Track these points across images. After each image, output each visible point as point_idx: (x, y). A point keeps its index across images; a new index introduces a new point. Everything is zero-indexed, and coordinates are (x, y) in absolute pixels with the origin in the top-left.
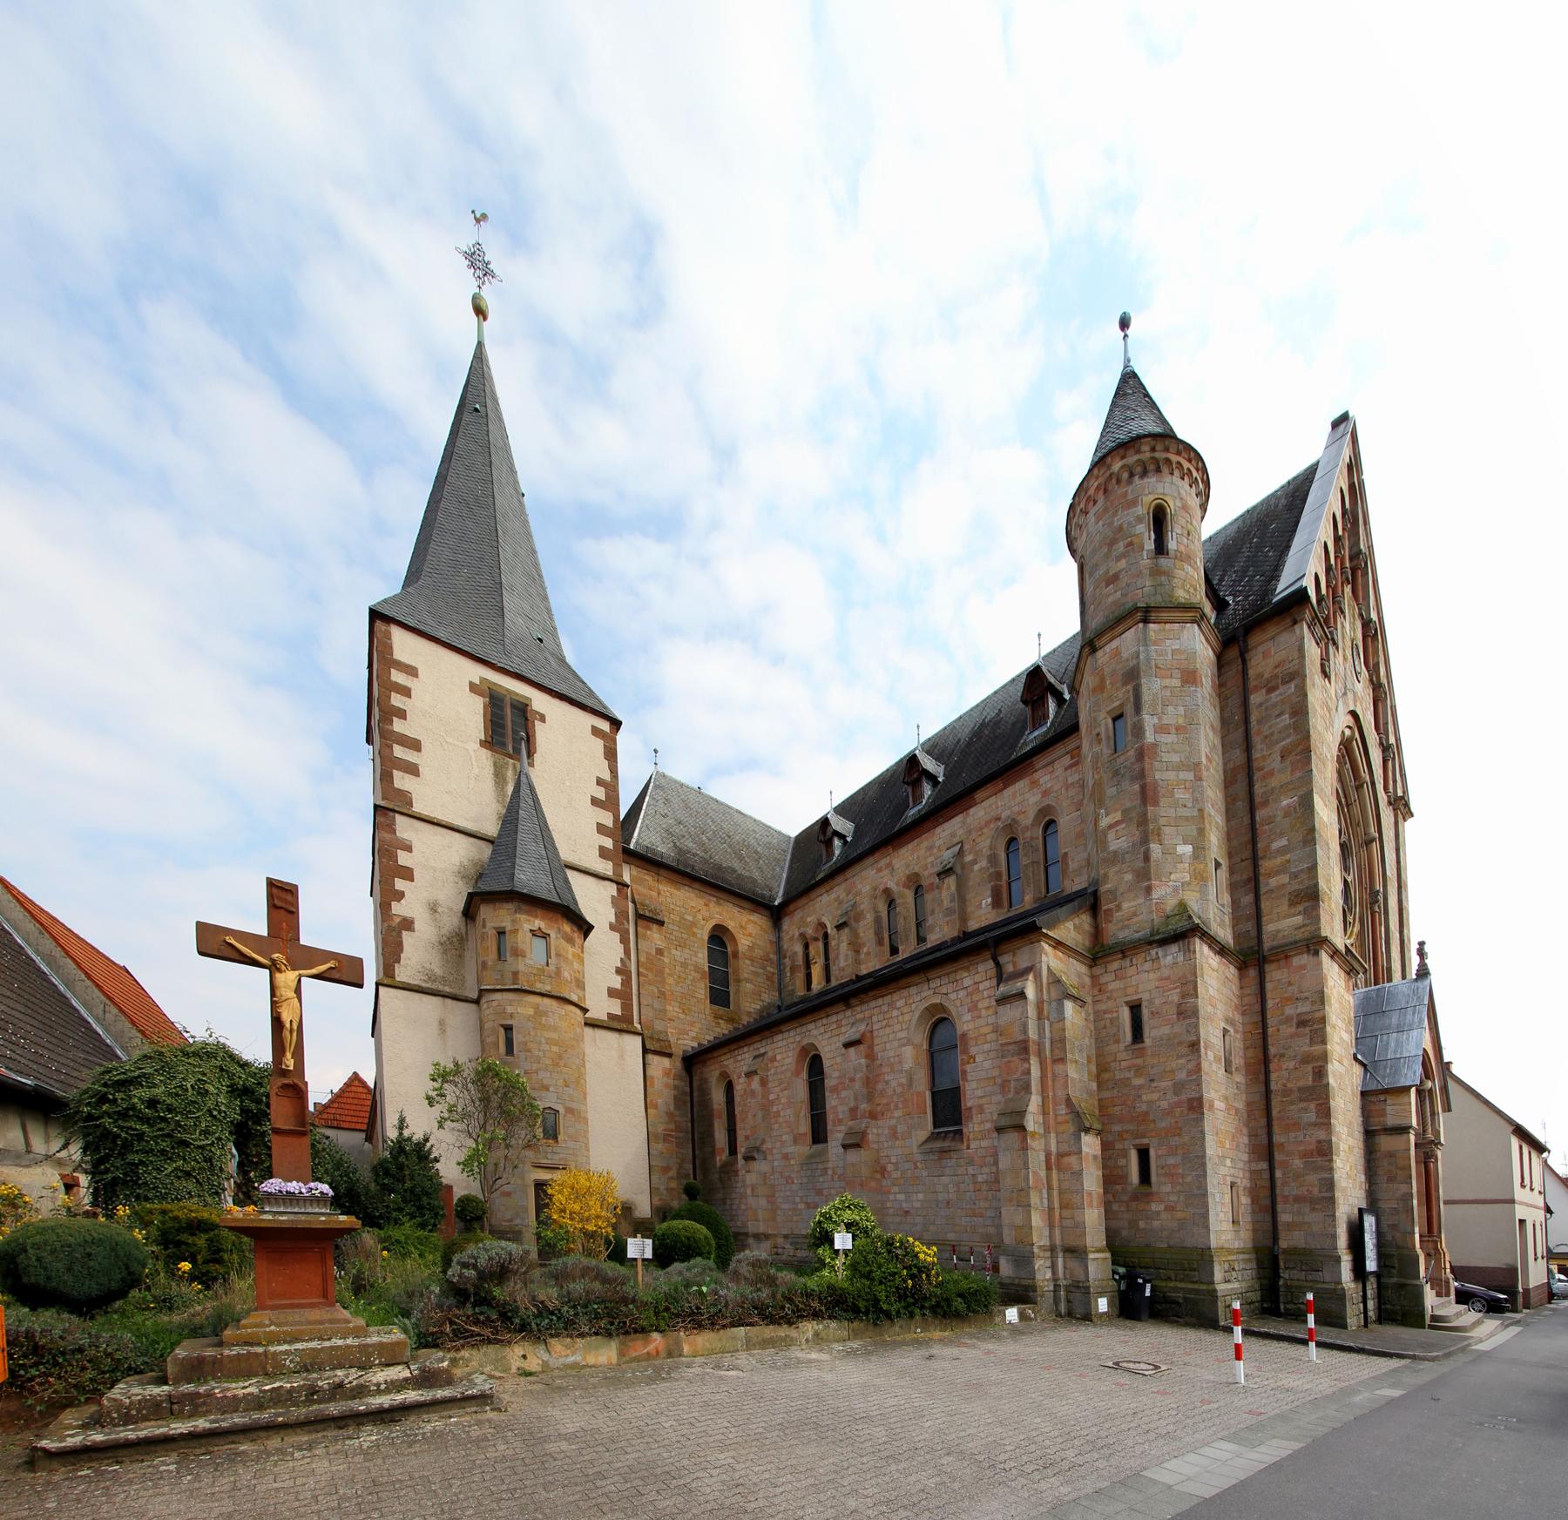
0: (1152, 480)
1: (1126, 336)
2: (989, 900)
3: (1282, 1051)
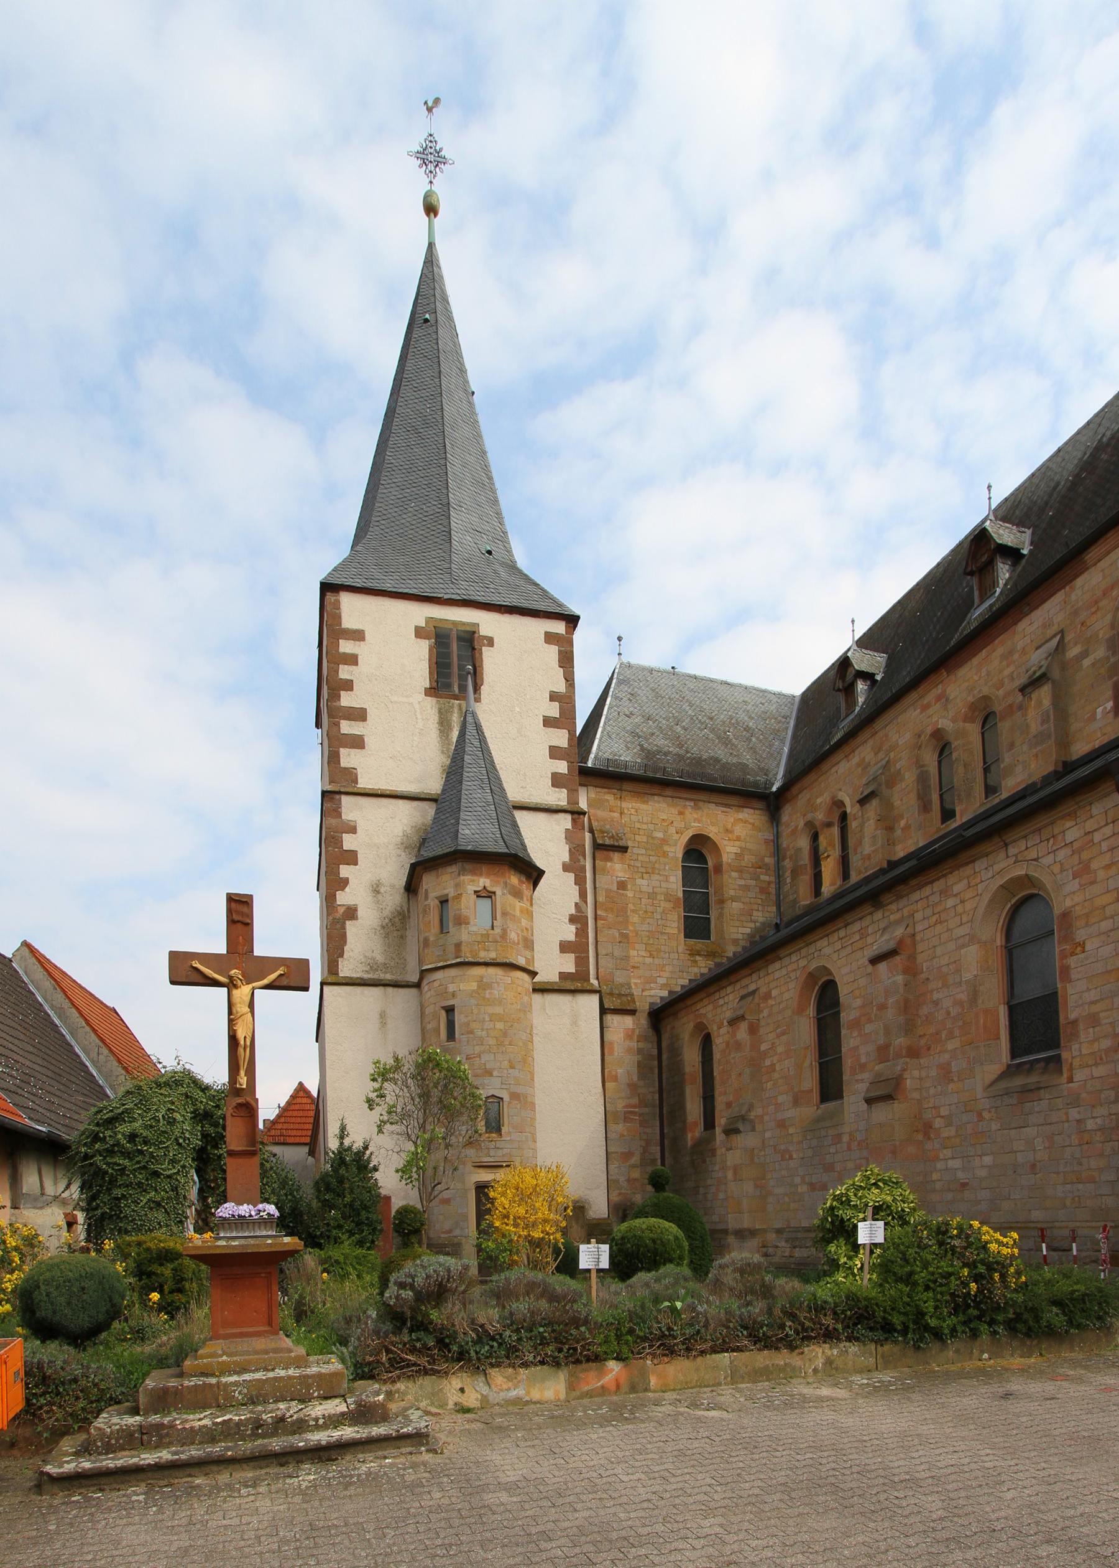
2: (1110, 705)
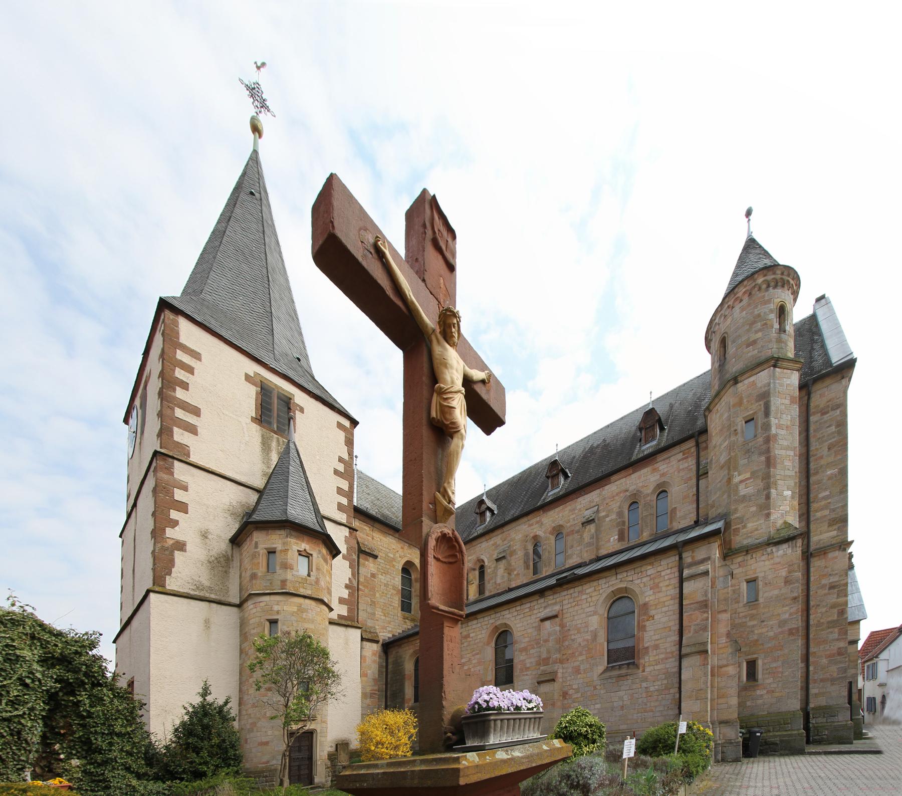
0: (779, 291)
1: (749, 220)
2: (616, 537)
3: (818, 603)
